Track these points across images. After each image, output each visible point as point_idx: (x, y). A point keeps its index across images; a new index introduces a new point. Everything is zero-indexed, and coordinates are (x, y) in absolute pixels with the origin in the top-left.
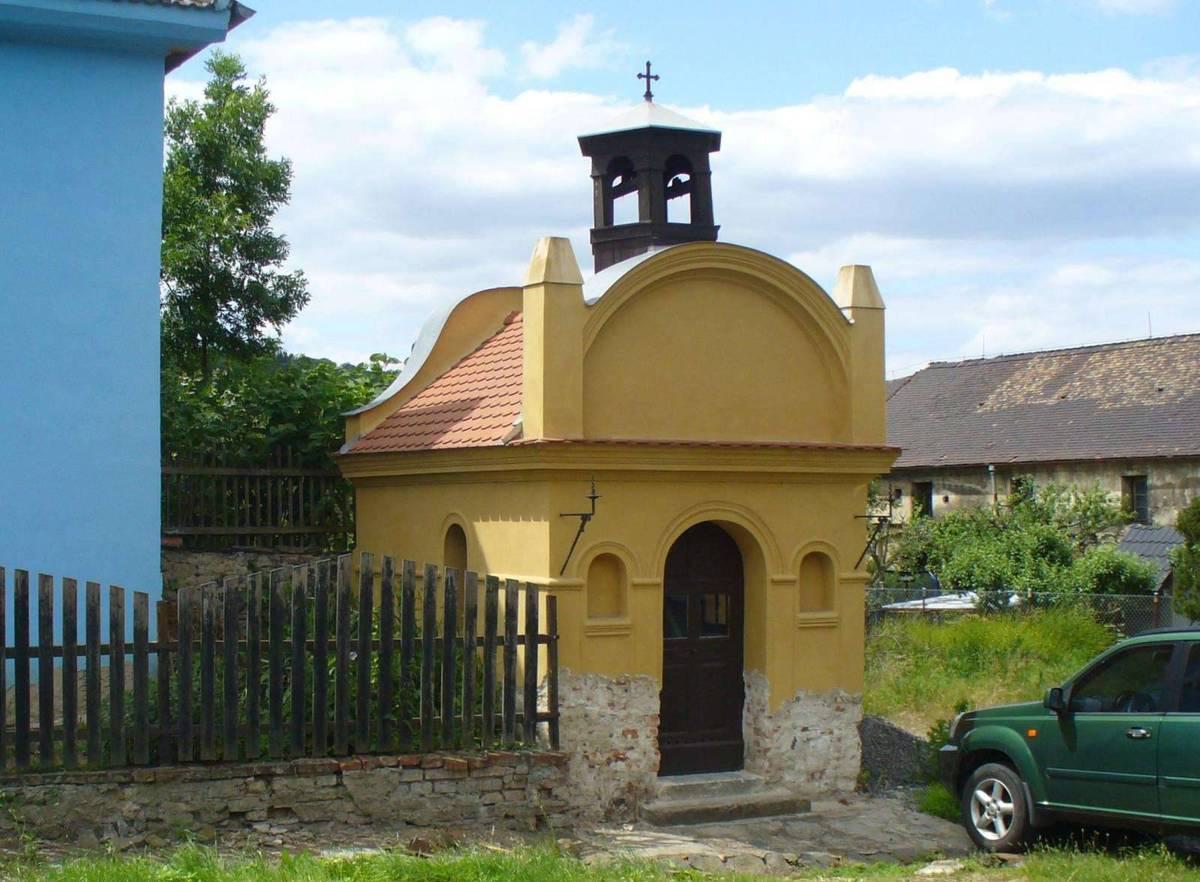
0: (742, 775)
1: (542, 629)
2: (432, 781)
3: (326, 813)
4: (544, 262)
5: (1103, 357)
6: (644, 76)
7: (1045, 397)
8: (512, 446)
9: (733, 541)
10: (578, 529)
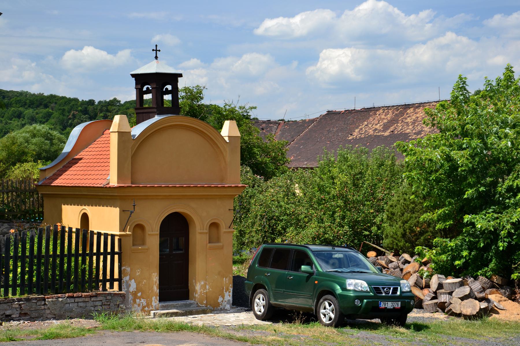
0: (188, 302)
1: (116, 250)
2: (78, 302)
3: (40, 314)
4: (118, 124)
5: (414, 110)
6: (155, 50)
7: (383, 131)
8: (106, 187)
9: (185, 218)
10: (59, 341)
